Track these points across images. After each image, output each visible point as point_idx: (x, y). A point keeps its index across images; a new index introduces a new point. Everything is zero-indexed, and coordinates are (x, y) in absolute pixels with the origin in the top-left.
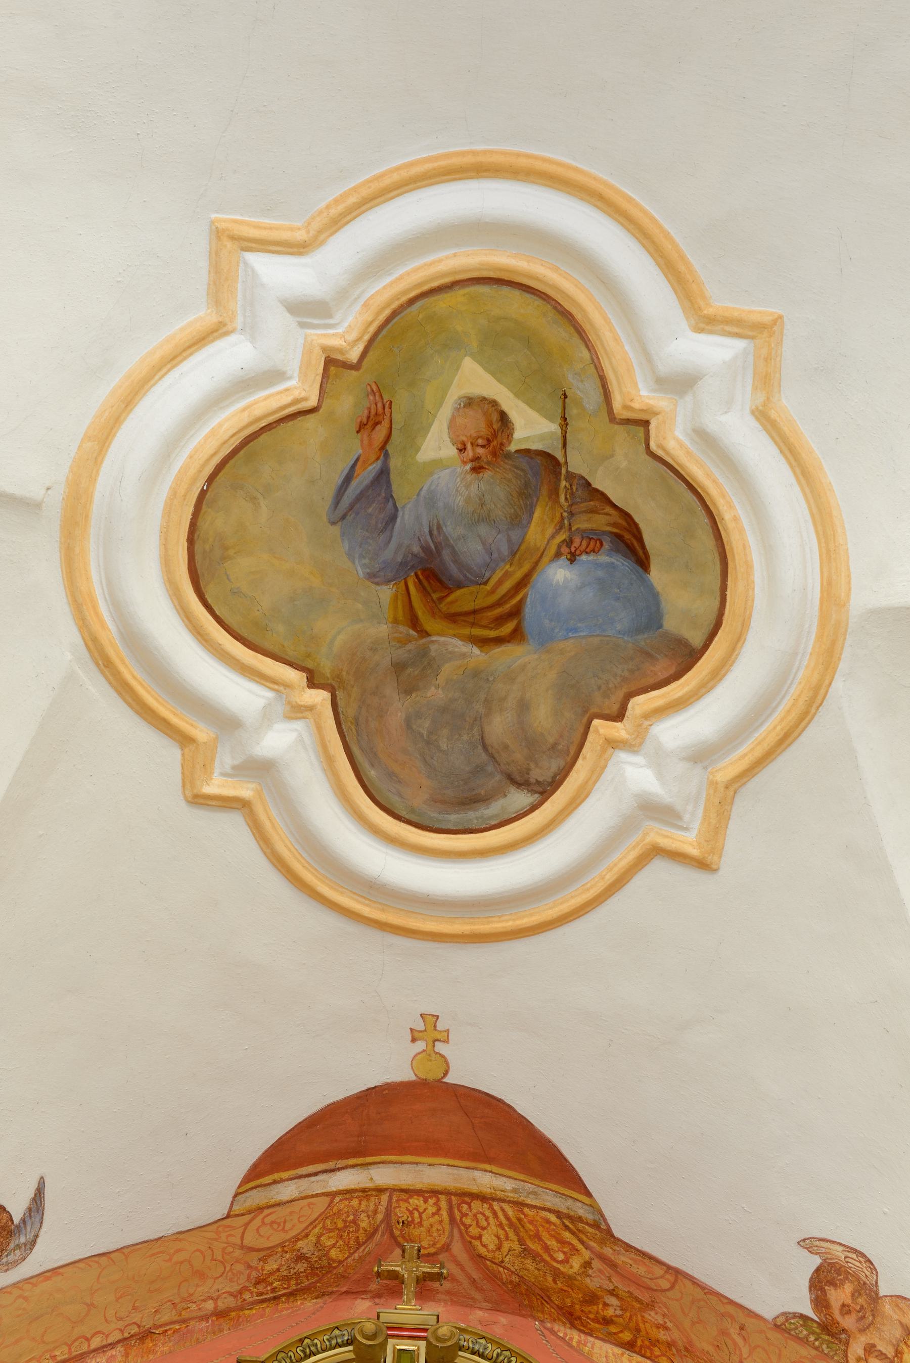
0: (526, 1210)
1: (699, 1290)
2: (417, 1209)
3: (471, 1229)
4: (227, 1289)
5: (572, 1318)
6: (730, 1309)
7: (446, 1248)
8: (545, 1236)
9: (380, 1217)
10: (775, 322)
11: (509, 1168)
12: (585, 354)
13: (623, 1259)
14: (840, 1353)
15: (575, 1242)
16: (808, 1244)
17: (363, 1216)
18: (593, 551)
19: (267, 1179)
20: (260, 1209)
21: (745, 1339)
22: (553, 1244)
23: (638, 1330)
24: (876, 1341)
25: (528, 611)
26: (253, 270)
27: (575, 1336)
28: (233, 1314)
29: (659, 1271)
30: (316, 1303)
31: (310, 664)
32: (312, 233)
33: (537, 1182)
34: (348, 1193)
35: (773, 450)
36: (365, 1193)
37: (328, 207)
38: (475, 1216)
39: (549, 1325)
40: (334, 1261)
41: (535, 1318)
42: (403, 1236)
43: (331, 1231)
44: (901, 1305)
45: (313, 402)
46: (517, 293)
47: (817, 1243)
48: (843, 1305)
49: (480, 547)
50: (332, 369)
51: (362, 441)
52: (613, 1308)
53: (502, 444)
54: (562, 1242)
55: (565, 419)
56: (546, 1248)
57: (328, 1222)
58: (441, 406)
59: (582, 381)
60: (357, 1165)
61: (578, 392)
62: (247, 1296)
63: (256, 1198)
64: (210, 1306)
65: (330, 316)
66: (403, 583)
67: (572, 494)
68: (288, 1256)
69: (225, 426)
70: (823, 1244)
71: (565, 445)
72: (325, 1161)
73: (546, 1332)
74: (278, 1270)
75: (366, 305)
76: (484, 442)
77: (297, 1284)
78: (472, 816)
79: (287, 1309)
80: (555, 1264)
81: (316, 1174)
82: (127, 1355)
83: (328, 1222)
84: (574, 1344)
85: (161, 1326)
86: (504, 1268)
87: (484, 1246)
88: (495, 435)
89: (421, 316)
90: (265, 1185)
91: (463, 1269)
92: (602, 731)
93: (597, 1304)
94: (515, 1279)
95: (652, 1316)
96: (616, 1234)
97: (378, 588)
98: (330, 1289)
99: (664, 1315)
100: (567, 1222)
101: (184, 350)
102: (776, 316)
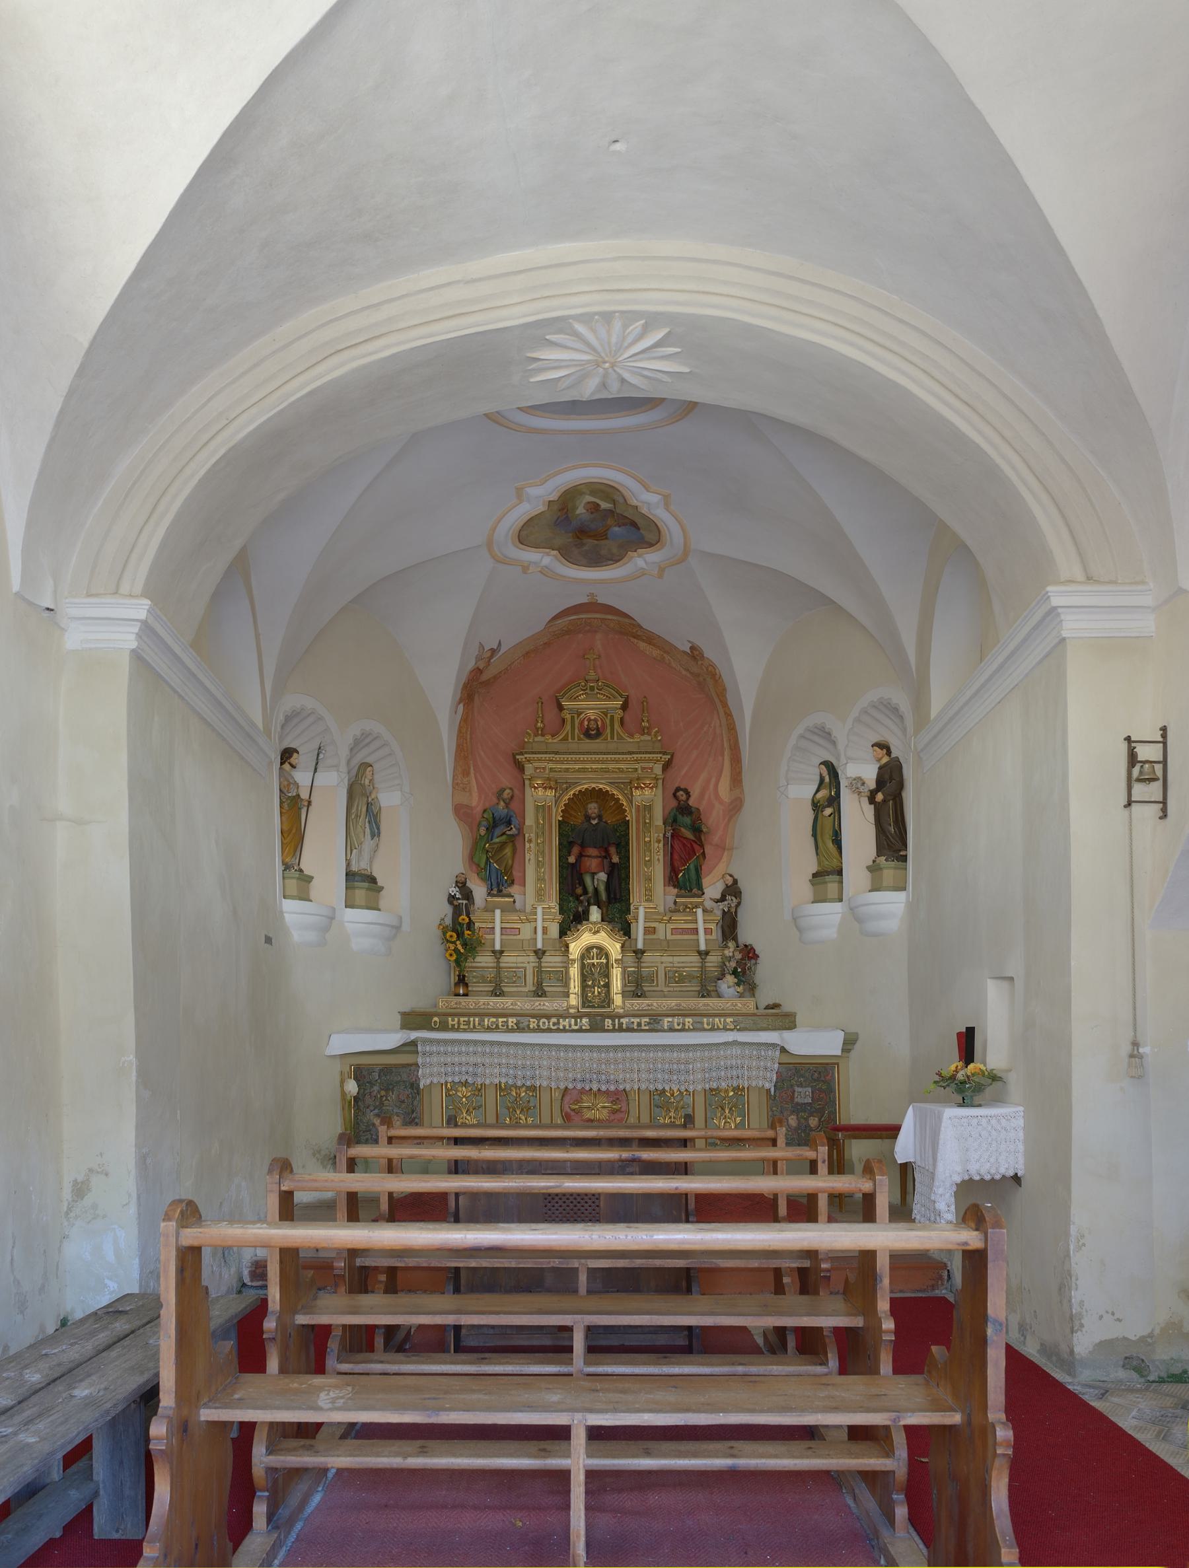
82: (524, 659)
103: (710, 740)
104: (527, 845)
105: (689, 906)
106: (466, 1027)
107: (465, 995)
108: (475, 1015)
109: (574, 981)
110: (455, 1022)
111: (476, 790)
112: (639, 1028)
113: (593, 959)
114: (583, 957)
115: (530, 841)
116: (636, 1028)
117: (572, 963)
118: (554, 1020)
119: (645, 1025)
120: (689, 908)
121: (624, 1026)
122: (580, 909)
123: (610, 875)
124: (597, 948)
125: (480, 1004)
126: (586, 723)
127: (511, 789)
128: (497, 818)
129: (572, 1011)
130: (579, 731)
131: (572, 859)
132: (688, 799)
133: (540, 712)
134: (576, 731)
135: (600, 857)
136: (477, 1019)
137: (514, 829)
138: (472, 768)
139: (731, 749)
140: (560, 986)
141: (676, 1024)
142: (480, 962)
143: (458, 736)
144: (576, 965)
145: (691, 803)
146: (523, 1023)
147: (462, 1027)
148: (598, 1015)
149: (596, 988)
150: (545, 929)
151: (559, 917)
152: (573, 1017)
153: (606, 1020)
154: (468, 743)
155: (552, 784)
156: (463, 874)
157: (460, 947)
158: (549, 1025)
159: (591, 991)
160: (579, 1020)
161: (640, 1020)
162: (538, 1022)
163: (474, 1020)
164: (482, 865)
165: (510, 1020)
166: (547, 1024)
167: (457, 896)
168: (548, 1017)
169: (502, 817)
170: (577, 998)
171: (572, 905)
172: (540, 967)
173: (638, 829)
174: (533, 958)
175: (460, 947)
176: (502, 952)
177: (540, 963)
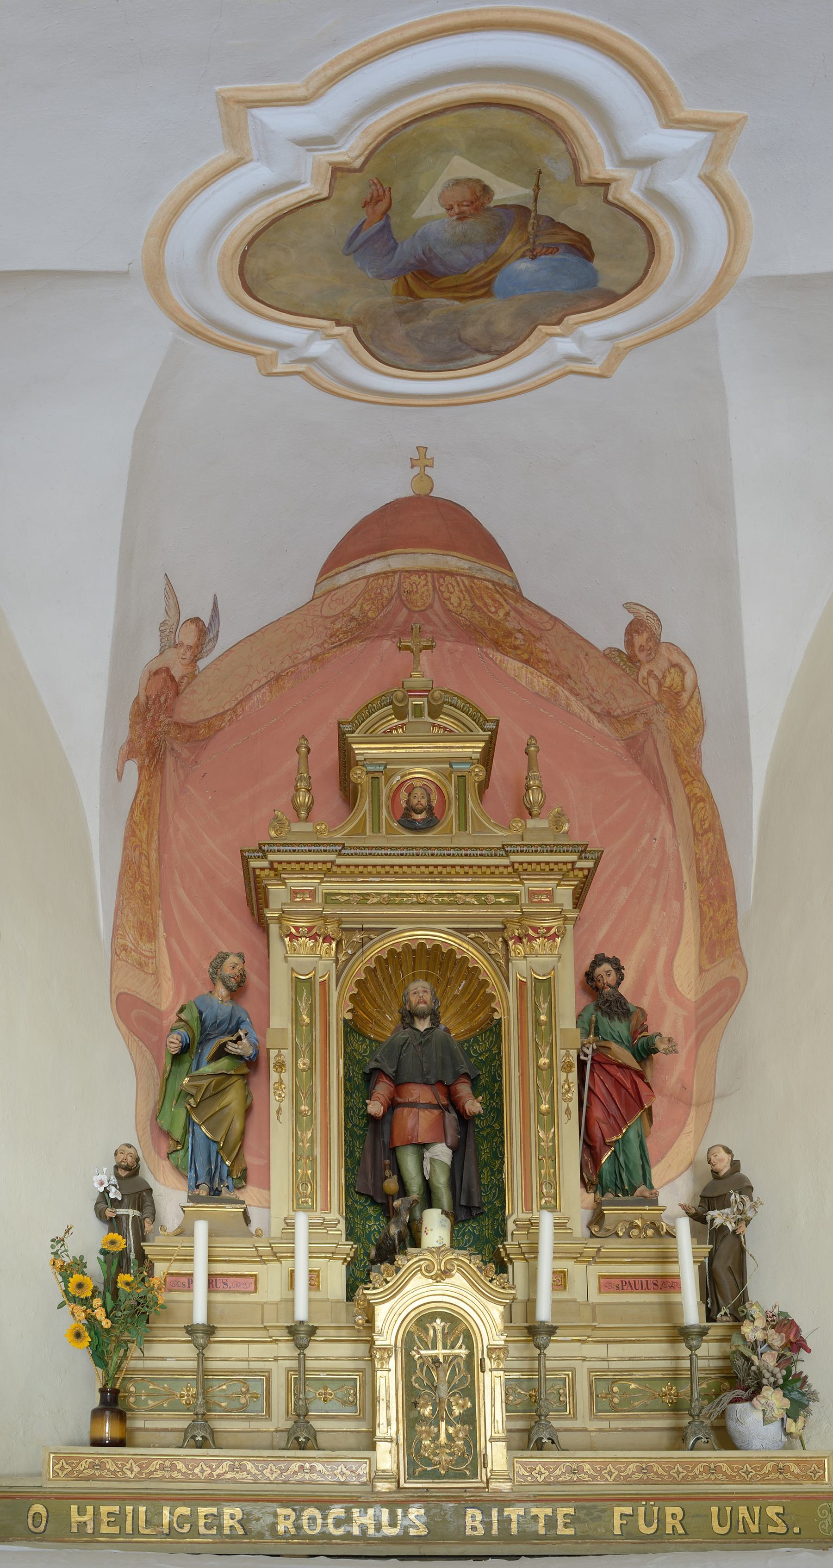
0: (476, 581)
1: (566, 631)
2: (415, 583)
3: (444, 594)
4: (316, 643)
5: (497, 645)
6: (582, 643)
7: (431, 606)
8: (485, 597)
9: (394, 589)
10: (738, 121)
11: (467, 554)
12: (562, 146)
13: (527, 610)
14: (635, 673)
15: (502, 600)
16: (628, 606)
17: (385, 589)
18: (551, 253)
19: (332, 573)
20: (329, 592)
21: (587, 661)
22: (489, 601)
23: (532, 653)
24: (654, 669)
25: (496, 284)
26: (261, 121)
27: (498, 656)
28: (320, 657)
29: (546, 618)
30: (362, 645)
31: (337, 317)
32: (311, 90)
33: (482, 563)
34: (377, 575)
35: (710, 197)
36: (386, 574)
37: (324, 69)
38: (447, 585)
39: (485, 650)
40: (370, 619)
41: (477, 645)
42: (407, 600)
43: (368, 600)
44: (671, 649)
45: (325, 194)
46: (504, 111)
47: (633, 606)
48: (641, 646)
49: (462, 257)
50: (339, 174)
51: (367, 212)
52: (519, 640)
53: (483, 203)
54: (494, 600)
55: (538, 186)
56: (486, 605)
57: (366, 595)
58: (433, 186)
59: (556, 163)
60: (381, 557)
61: (552, 170)
62: (326, 645)
63: (327, 585)
64: (308, 654)
65: (335, 143)
66: (402, 279)
67: (538, 226)
68: (346, 619)
69: (256, 216)
70: (636, 607)
71: (536, 200)
72: (363, 556)
73: (483, 654)
74: (341, 628)
75: (365, 132)
76: (469, 203)
77: (352, 635)
78: (451, 365)
79: (348, 651)
80: (490, 614)
81: (358, 566)
82: (271, 692)
83: (366, 595)
84: (498, 662)
85: (285, 670)
86: (462, 617)
87: (451, 604)
88: (478, 199)
89: (415, 134)
90: (331, 577)
91: (440, 619)
92: (543, 330)
93: (511, 638)
94: (468, 623)
95: (540, 645)
96: (524, 596)
97: (384, 281)
98: (369, 636)
99: (547, 645)
100: (498, 588)
101: (213, 178)
102: (741, 116)
103: (655, 866)
104: (274, 1076)
105: (639, 1222)
106: (115, 1530)
107: (120, 1443)
108: (137, 1498)
109: (388, 1407)
110: (88, 1518)
111: (169, 973)
112: (552, 1532)
113: (434, 1347)
114: (409, 1342)
115: (280, 1066)
116: (542, 1532)
117: (382, 1358)
118: (337, 1511)
119: (566, 1525)
120: (637, 1226)
121: (514, 1528)
122: (394, 1230)
123: (458, 1151)
124: (445, 1317)
125: (152, 1468)
126: (403, 796)
127: (240, 955)
128: (208, 1023)
129: (382, 1486)
130: (388, 812)
131: (375, 1108)
132: (618, 984)
133: (303, 769)
134: (384, 813)
135: (438, 1107)
136: (142, 1509)
137: (244, 1041)
138: (161, 925)
139: (700, 880)
140: (348, 1418)
141: (641, 1522)
142: (163, 1359)
143: (126, 840)
144: (391, 1364)
145: (623, 989)
146: (258, 1520)
147: (104, 1529)
148: (449, 1499)
149: (443, 1425)
150: (315, 1275)
151: (347, 1248)
152: (385, 1504)
153: (470, 1512)
154: (153, 867)
155: (331, 929)
156: (129, 1146)
157: (100, 1314)
158: (324, 1525)
159: (428, 1433)
160: (400, 1511)
161: (554, 1512)
162: (299, 1518)
163: (135, 1513)
164: (178, 1134)
165: (227, 1511)
166: (319, 1521)
167: (112, 1196)
168: (323, 1503)
169: (220, 1018)
170: (394, 1452)
171: (373, 1225)
172: (302, 1370)
173: (522, 1037)
174: (286, 1349)
175: (100, 1314)
176: (210, 1330)
177: (302, 1359)
